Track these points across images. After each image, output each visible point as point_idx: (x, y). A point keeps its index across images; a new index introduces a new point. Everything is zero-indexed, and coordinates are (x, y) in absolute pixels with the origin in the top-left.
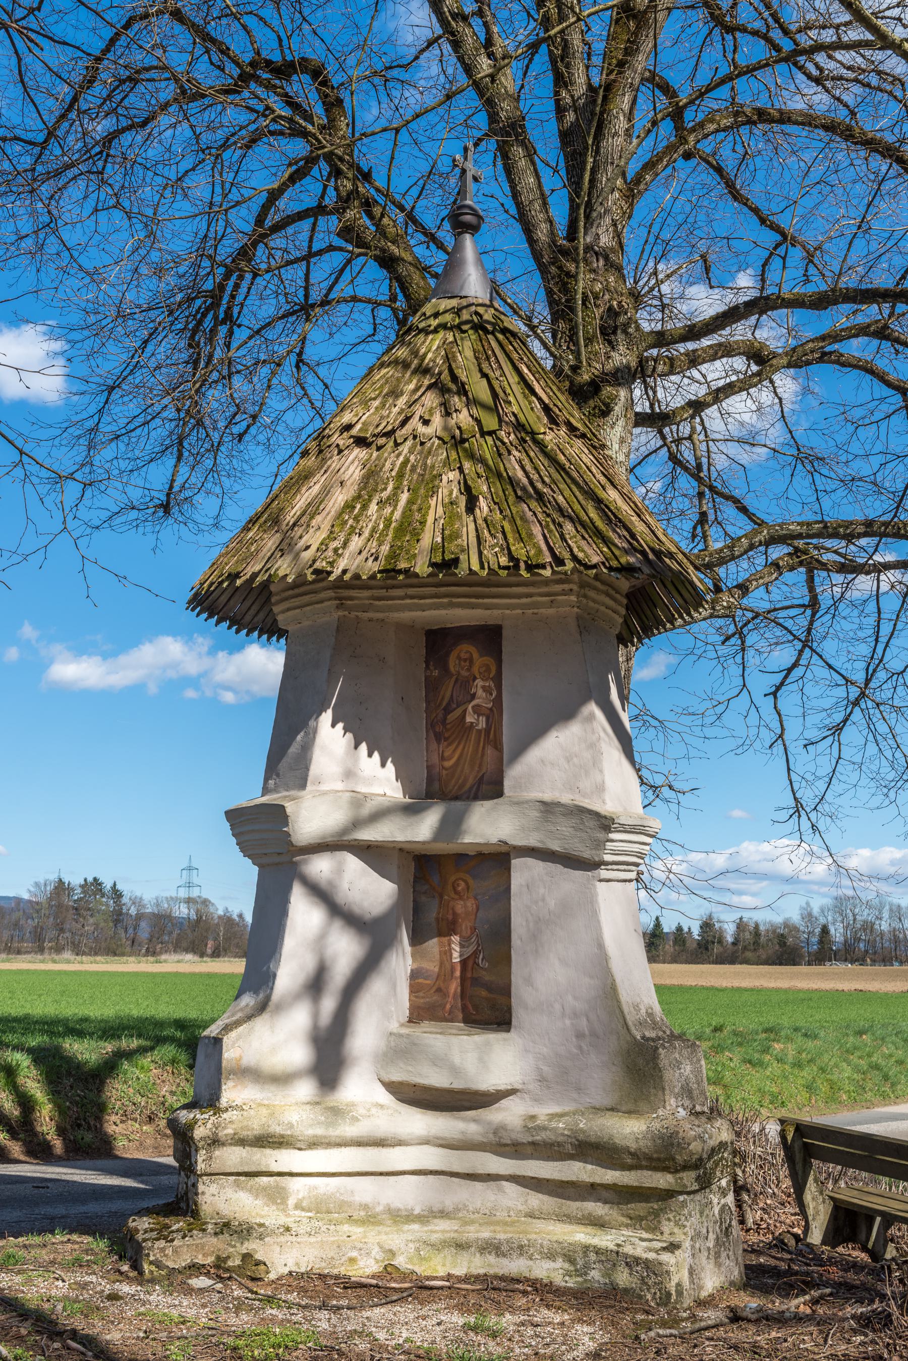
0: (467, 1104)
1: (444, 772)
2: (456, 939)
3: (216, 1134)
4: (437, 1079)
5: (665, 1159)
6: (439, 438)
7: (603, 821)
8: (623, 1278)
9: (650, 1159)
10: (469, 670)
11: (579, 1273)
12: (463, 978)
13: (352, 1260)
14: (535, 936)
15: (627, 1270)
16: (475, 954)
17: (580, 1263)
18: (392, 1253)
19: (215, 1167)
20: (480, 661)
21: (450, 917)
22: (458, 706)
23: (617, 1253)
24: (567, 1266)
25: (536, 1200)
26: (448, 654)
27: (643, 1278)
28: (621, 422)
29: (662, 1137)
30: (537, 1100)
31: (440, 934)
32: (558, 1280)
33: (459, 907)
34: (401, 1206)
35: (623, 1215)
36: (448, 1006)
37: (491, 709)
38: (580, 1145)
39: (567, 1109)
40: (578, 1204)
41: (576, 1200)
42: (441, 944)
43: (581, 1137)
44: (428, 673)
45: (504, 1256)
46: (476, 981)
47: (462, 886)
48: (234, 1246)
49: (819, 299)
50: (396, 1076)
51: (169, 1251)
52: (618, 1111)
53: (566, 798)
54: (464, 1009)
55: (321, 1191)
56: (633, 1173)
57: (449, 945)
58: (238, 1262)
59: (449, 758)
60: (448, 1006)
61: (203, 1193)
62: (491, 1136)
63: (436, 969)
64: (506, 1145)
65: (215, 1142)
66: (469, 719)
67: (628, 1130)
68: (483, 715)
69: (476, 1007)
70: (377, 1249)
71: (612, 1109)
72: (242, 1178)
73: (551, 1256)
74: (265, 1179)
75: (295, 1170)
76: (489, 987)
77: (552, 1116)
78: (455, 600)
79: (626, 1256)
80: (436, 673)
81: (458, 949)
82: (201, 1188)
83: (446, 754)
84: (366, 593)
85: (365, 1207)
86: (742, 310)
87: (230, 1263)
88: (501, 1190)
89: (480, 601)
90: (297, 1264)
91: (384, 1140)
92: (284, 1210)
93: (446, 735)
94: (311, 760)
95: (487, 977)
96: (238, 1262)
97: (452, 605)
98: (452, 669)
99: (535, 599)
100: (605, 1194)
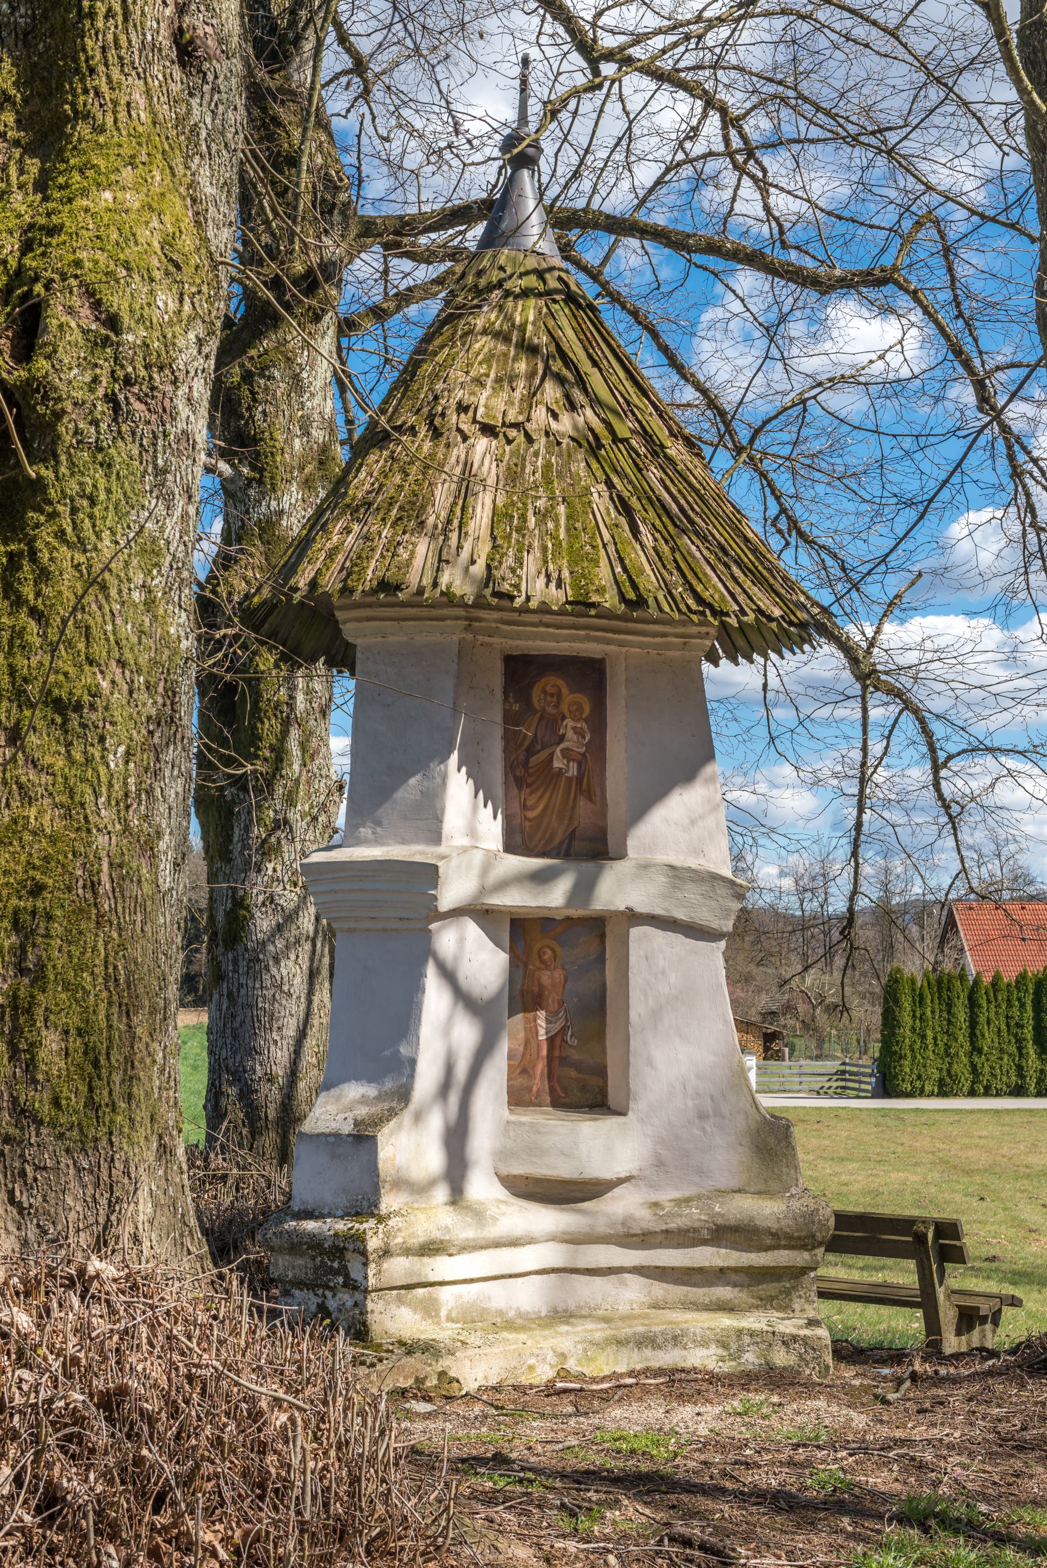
0: (579, 1195)
1: (527, 824)
2: (542, 1014)
3: (387, 1244)
4: (563, 1170)
5: (806, 1237)
6: (573, 439)
7: (738, 889)
8: (781, 1358)
9: (791, 1238)
10: (556, 706)
11: (733, 1357)
12: (550, 1058)
13: (531, 1368)
14: (656, 1015)
15: (783, 1349)
16: (563, 1030)
17: (734, 1346)
18: (563, 1356)
19: (385, 1282)
20: (570, 698)
21: (536, 989)
22: (543, 748)
23: (774, 1333)
24: (721, 1352)
25: (660, 1290)
26: (530, 686)
27: (801, 1355)
28: (331, 332)
29: (803, 1216)
30: (653, 1186)
31: (525, 1010)
32: (712, 1365)
33: (546, 978)
34: (530, 1309)
35: (753, 1297)
36: (535, 1089)
37: (583, 755)
38: (717, 1230)
39: (687, 1193)
40: (705, 1290)
41: (703, 1286)
42: (527, 1021)
43: (720, 1221)
44: (508, 706)
45: (660, 1348)
46: (564, 1060)
47: (548, 954)
48: (430, 1365)
49: (568, 218)
50: (505, 1171)
51: (374, 1377)
52: (746, 1192)
53: (692, 863)
54: (552, 1091)
55: (465, 1299)
56: (770, 1253)
57: (535, 1020)
58: (435, 1382)
59: (533, 808)
60: (535, 1089)
61: (372, 1311)
62: (619, 1227)
63: (521, 1049)
64: (636, 1235)
65: (386, 1253)
66: (557, 764)
67: (768, 1211)
68: (574, 760)
69: (565, 1089)
70: (551, 1354)
71: (739, 1191)
72: (403, 1292)
73: (704, 1343)
74: (420, 1291)
75: (447, 1279)
76: (578, 1067)
77: (679, 1202)
78: (592, 633)
79: (783, 1335)
80: (516, 707)
81: (544, 1025)
82: (370, 1306)
83: (529, 803)
84: (496, 615)
85: (501, 1313)
86: (475, 211)
87: (428, 1384)
88: (623, 1283)
89: (617, 636)
90: (486, 1378)
91: (518, 1239)
92: (438, 1323)
93: (529, 781)
94: (443, 810)
95: (576, 1056)
96: (435, 1382)
97: (589, 639)
98: (536, 704)
99: (669, 639)
100: (734, 1277)
